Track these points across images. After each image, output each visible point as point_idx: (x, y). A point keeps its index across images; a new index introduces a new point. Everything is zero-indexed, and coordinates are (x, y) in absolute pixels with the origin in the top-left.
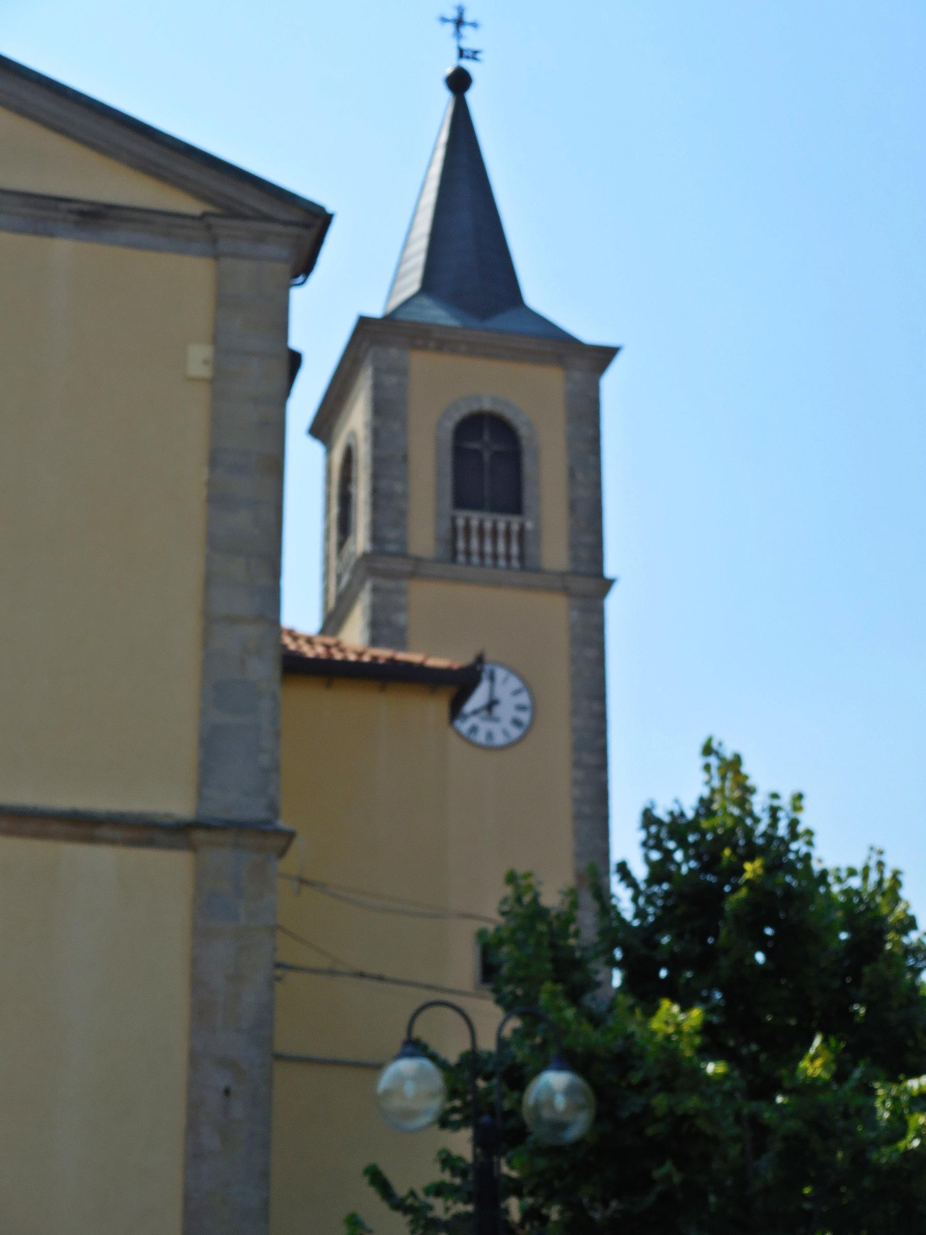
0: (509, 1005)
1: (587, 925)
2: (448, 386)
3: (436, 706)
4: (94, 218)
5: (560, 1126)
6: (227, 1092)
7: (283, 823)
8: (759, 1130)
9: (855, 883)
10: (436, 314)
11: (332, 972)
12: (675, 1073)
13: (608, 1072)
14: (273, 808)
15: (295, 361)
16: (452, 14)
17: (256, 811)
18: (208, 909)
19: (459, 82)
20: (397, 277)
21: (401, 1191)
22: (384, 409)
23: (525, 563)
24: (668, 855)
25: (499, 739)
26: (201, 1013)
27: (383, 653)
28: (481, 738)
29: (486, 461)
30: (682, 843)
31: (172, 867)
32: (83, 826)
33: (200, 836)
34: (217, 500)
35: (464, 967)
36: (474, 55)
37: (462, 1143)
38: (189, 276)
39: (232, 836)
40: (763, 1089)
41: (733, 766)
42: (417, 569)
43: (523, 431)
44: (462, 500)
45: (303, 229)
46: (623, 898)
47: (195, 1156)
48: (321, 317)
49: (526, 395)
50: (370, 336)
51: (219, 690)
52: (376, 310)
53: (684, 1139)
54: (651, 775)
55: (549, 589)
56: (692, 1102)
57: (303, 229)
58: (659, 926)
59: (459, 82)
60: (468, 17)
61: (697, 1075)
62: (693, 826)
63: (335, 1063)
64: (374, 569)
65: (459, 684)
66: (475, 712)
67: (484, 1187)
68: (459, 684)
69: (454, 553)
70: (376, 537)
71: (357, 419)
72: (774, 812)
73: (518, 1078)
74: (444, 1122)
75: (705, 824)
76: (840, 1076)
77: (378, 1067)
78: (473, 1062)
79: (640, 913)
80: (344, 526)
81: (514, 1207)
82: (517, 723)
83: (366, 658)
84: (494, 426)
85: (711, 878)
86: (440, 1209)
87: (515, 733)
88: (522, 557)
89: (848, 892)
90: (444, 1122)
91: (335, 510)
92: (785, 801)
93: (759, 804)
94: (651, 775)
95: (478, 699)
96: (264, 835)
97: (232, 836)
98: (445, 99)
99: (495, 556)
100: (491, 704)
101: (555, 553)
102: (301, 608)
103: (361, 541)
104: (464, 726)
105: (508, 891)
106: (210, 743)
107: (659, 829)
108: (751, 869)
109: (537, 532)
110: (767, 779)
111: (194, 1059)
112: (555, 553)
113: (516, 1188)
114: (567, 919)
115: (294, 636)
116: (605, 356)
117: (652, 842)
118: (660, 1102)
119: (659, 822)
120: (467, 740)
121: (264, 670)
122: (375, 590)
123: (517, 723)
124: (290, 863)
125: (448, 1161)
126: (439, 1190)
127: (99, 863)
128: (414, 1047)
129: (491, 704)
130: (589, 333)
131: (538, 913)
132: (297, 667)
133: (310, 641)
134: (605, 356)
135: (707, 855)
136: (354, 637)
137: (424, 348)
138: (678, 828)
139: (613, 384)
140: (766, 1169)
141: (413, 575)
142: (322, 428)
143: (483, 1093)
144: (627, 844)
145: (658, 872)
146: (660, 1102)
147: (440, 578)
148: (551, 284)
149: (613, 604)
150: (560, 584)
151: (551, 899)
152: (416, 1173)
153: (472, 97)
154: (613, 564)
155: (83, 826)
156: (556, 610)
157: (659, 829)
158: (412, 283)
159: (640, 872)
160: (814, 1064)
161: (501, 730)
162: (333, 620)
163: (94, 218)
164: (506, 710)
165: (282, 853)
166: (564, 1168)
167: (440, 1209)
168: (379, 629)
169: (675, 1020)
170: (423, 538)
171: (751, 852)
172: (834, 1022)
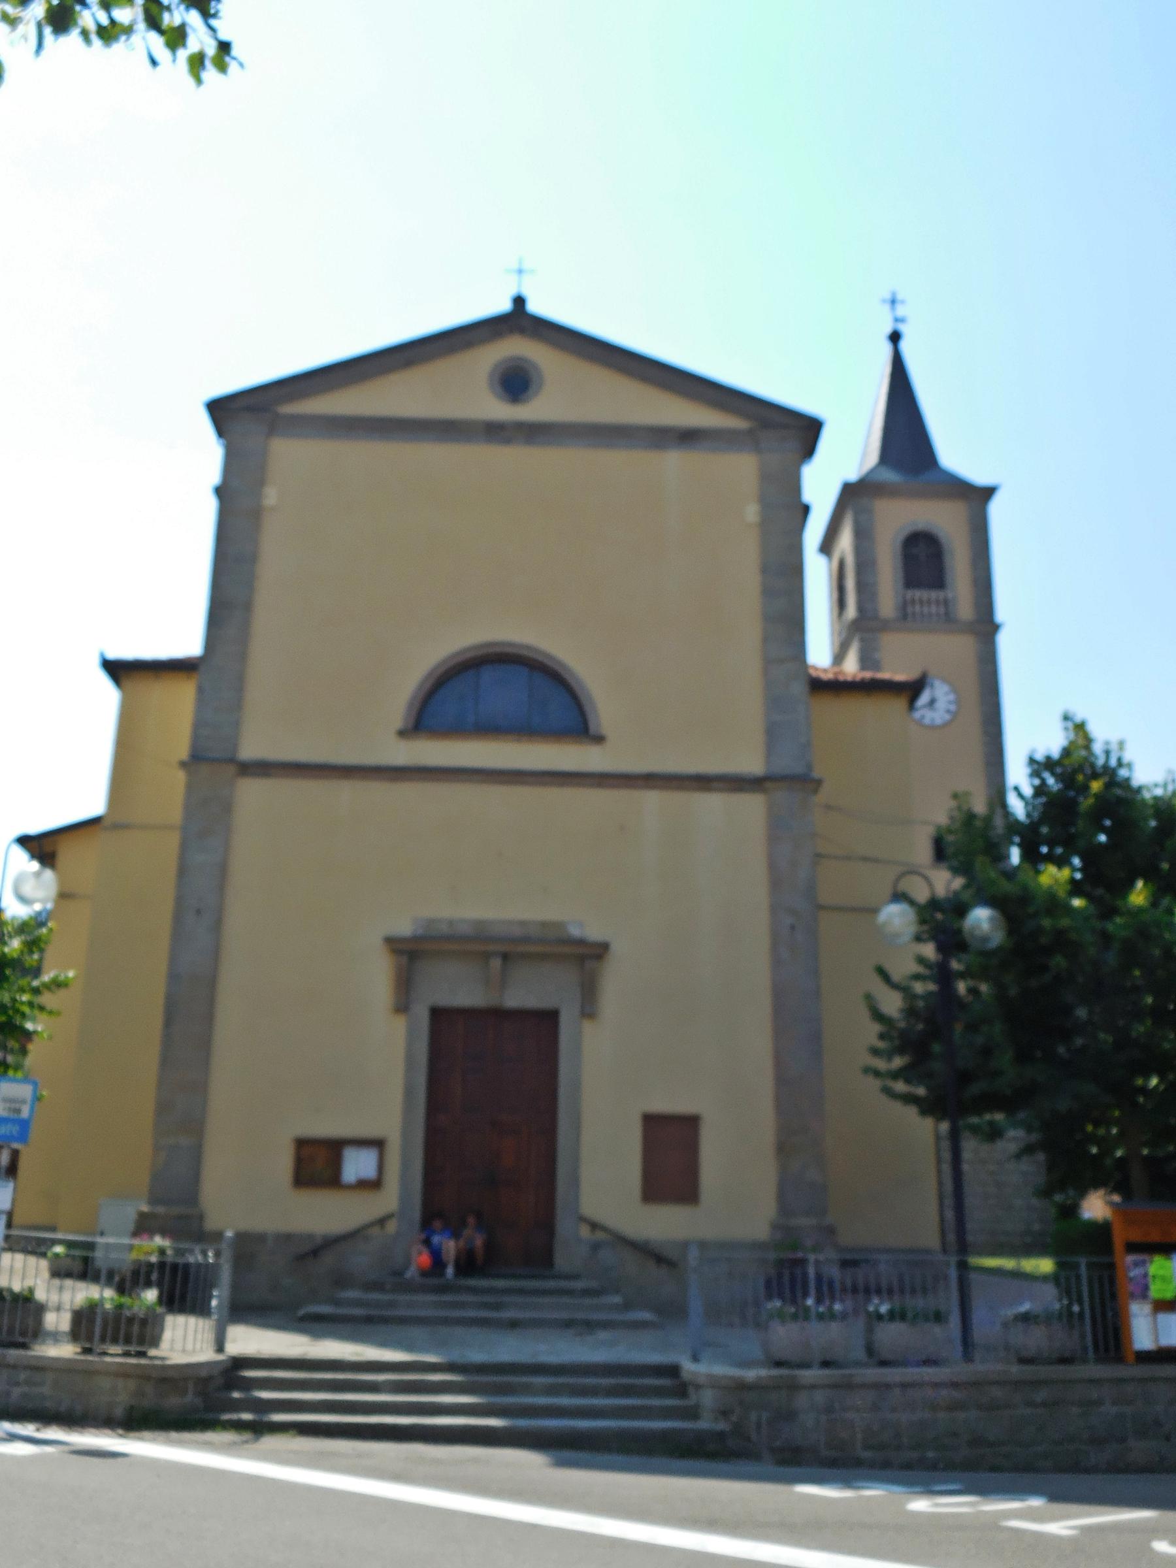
0: (956, 871)
1: (999, 822)
2: (897, 517)
3: (895, 706)
4: (688, 437)
5: (985, 939)
6: (793, 927)
7: (816, 774)
8: (1106, 938)
9: (1159, 792)
10: (890, 476)
11: (848, 858)
12: (1054, 905)
13: (1015, 906)
14: (810, 767)
15: (806, 509)
16: (888, 296)
17: (799, 769)
18: (776, 828)
19: (895, 337)
20: (864, 455)
21: (896, 977)
22: (862, 536)
23: (948, 620)
24: (1043, 781)
25: (938, 721)
26: (776, 883)
27: (868, 675)
28: (927, 721)
29: (923, 559)
30: (1053, 774)
31: (753, 806)
32: (703, 782)
33: (768, 785)
34: (768, 592)
35: (923, 852)
37: (929, 950)
38: (741, 470)
39: (787, 783)
40: (1108, 912)
41: (1080, 727)
42: (886, 626)
45: (805, 432)
46: (1018, 808)
47: (777, 963)
48: (822, 482)
50: (853, 495)
51: (775, 702)
52: (853, 476)
53: (1062, 941)
54: (1030, 735)
56: (1065, 922)
57: (805, 432)
58: (1042, 821)
59: (895, 337)
60: (899, 297)
61: (1069, 910)
62: (1058, 763)
63: (854, 910)
64: (861, 627)
65: (912, 690)
66: (924, 706)
67: (943, 975)
68: (912, 690)
70: (861, 608)
71: (845, 542)
72: (1107, 753)
73: (960, 909)
74: (918, 939)
75: (1066, 762)
76: (1154, 904)
77: (875, 911)
78: (934, 904)
79: (1028, 815)
80: (841, 603)
81: (961, 987)
83: (858, 678)
84: (928, 537)
85: (1072, 793)
86: (919, 988)
87: (947, 717)
89: (1156, 798)
90: (918, 939)
91: (835, 595)
92: (1114, 747)
93: (1098, 748)
94: (1030, 735)
95: (924, 698)
96: (804, 782)
97: (787, 783)
98: (886, 349)
100: (932, 702)
101: (965, 609)
102: (820, 651)
103: (851, 612)
104: (917, 715)
105: (953, 804)
106: (772, 734)
107: (1039, 767)
108: (1096, 786)
110: (1102, 734)
112: (965, 609)
113: (962, 975)
114: (988, 820)
115: (816, 669)
116: (988, 492)
117: (1035, 774)
118: (1046, 923)
119: (1037, 763)
120: (919, 723)
121: (799, 688)
122: (862, 640)
124: (822, 797)
125: (921, 960)
126: (917, 977)
128: (899, 896)
129: (932, 702)
130: (978, 476)
131: (970, 817)
132: (821, 687)
133: (825, 671)
134: (988, 492)
135: (1068, 779)
136: (851, 667)
138: (1049, 764)
139: (996, 510)
140: (1112, 959)
142: (826, 547)
143: (941, 922)
144: (1018, 775)
145: (1040, 791)
146: (1046, 923)
148: (956, 451)
151: (979, 807)
152: (903, 966)
153: (904, 345)
154: (1002, 613)
155: (703, 782)
156: (961, 646)
157: (1039, 767)
158: (873, 458)
159: (1028, 791)
160: (1139, 895)
161: (938, 716)
162: (839, 658)
163: (688, 437)
165: (815, 791)
166: (990, 964)
167: (919, 988)
168: (866, 661)
169: (1052, 876)
170: (887, 605)
171: (1095, 776)
172: (1150, 873)
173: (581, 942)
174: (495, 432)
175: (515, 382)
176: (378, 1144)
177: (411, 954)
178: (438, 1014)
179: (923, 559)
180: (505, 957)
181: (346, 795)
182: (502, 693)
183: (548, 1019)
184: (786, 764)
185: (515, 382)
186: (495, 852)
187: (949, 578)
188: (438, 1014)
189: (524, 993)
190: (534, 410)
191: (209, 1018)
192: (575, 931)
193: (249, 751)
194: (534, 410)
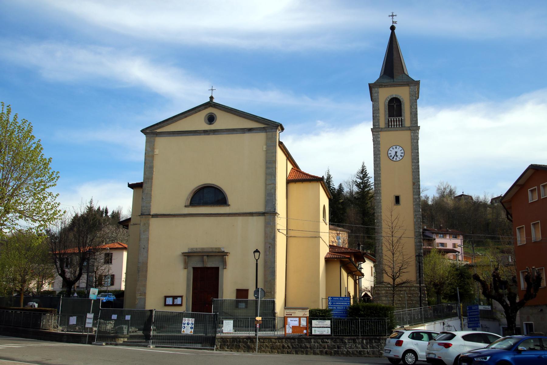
4: (250, 130)
16: (394, 14)
19: (393, 28)
29: (395, 108)
36: (396, 23)
38: (261, 137)
42: (382, 130)
43: (401, 100)
44: (390, 116)
49: (402, 93)
55: (407, 130)
59: (393, 28)
69: (389, 125)
82: (401, 156)
88: (402, 125)
99: (397, 125)
101: (407, 123)
109: (404, 119)
111: (265, 243)
123: (401, 156)
127: (255, 218)
130: (416, 79)
137: (382, 87)
141: (381, 131)
147: (386, 131)
149: (421, 132)
150: (409, 129)
153: (396, 31)
163: (250, 130)
164: (399, 154)
170: (382, 124)
173: (223, 252)
174: (206, 132)
175: (211, 119)
176: (181, 297)
177: (188, 256)
178: (194, 269)
179: (395, 108)
180: (208, 256)
181: (174, 220)
182: (209, 196)
183: (217, 269)
184: (269, 209)
185: (211, 119)
186: (205, 232)
187: (402, 114)
188: (194, 269)
189: (210, 264)
190: (216, 126)
191: (146, 271)
192: (223, 250)
193: (152, 213)
194: (216, 126)
